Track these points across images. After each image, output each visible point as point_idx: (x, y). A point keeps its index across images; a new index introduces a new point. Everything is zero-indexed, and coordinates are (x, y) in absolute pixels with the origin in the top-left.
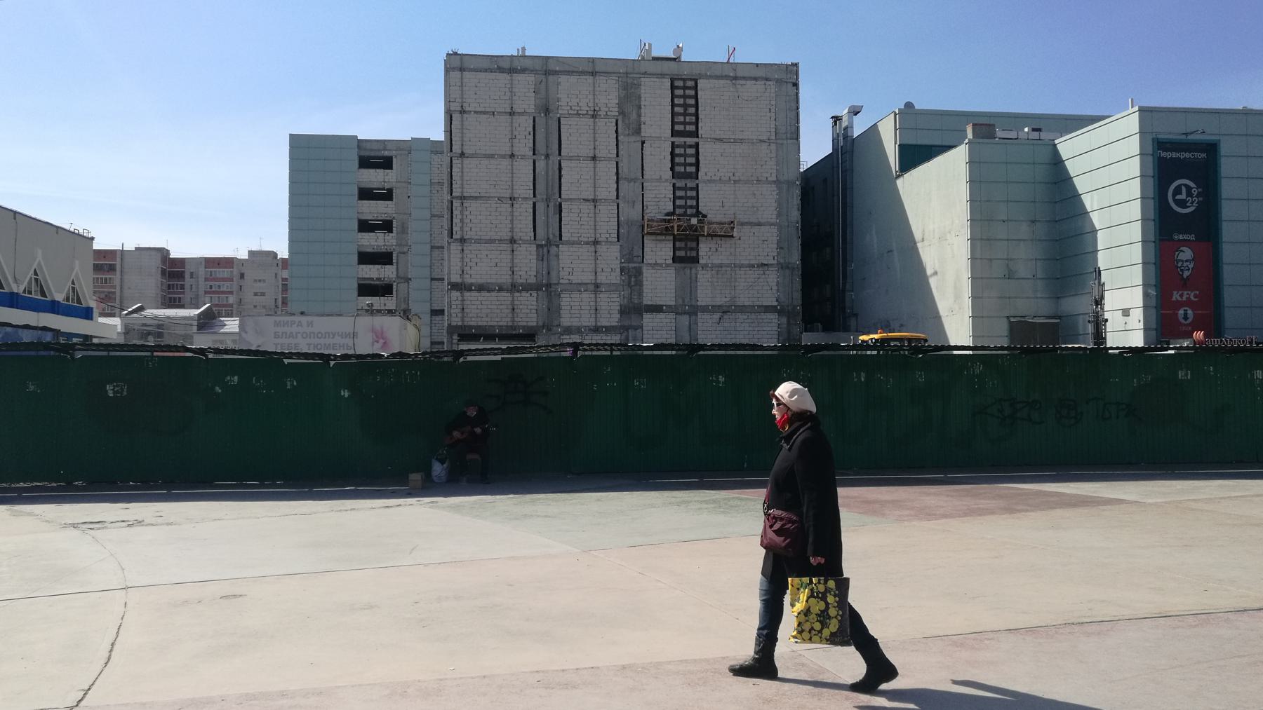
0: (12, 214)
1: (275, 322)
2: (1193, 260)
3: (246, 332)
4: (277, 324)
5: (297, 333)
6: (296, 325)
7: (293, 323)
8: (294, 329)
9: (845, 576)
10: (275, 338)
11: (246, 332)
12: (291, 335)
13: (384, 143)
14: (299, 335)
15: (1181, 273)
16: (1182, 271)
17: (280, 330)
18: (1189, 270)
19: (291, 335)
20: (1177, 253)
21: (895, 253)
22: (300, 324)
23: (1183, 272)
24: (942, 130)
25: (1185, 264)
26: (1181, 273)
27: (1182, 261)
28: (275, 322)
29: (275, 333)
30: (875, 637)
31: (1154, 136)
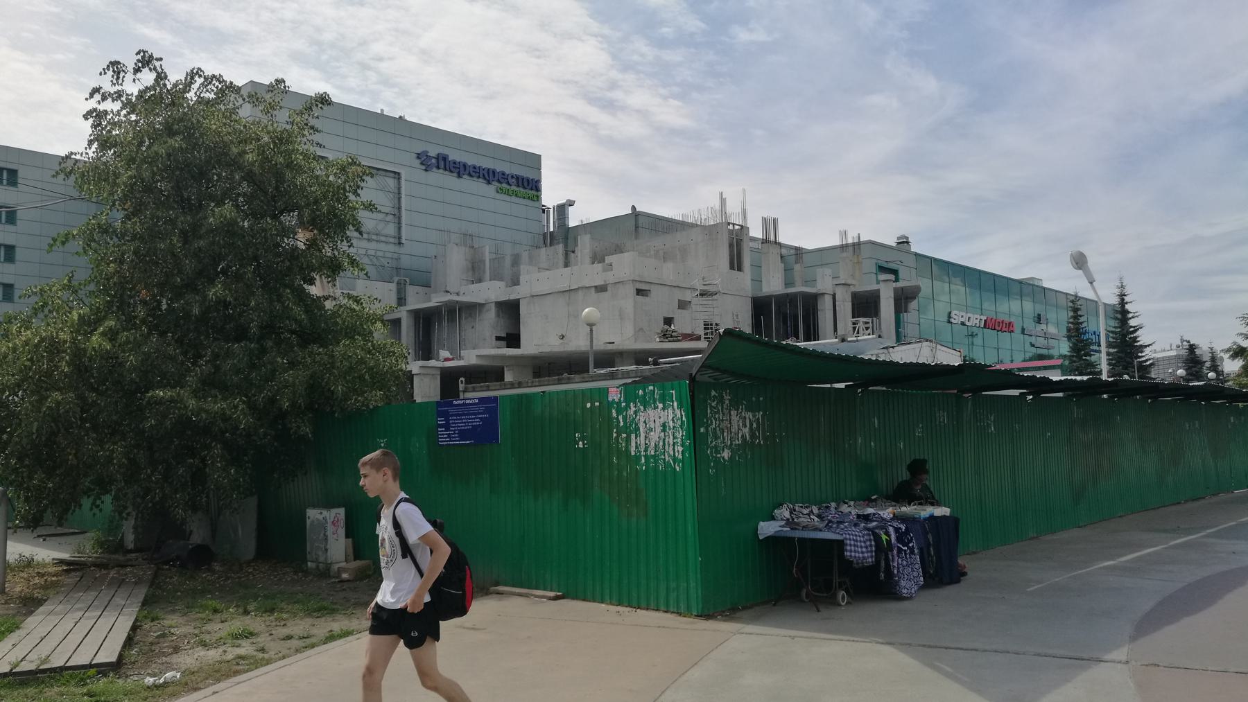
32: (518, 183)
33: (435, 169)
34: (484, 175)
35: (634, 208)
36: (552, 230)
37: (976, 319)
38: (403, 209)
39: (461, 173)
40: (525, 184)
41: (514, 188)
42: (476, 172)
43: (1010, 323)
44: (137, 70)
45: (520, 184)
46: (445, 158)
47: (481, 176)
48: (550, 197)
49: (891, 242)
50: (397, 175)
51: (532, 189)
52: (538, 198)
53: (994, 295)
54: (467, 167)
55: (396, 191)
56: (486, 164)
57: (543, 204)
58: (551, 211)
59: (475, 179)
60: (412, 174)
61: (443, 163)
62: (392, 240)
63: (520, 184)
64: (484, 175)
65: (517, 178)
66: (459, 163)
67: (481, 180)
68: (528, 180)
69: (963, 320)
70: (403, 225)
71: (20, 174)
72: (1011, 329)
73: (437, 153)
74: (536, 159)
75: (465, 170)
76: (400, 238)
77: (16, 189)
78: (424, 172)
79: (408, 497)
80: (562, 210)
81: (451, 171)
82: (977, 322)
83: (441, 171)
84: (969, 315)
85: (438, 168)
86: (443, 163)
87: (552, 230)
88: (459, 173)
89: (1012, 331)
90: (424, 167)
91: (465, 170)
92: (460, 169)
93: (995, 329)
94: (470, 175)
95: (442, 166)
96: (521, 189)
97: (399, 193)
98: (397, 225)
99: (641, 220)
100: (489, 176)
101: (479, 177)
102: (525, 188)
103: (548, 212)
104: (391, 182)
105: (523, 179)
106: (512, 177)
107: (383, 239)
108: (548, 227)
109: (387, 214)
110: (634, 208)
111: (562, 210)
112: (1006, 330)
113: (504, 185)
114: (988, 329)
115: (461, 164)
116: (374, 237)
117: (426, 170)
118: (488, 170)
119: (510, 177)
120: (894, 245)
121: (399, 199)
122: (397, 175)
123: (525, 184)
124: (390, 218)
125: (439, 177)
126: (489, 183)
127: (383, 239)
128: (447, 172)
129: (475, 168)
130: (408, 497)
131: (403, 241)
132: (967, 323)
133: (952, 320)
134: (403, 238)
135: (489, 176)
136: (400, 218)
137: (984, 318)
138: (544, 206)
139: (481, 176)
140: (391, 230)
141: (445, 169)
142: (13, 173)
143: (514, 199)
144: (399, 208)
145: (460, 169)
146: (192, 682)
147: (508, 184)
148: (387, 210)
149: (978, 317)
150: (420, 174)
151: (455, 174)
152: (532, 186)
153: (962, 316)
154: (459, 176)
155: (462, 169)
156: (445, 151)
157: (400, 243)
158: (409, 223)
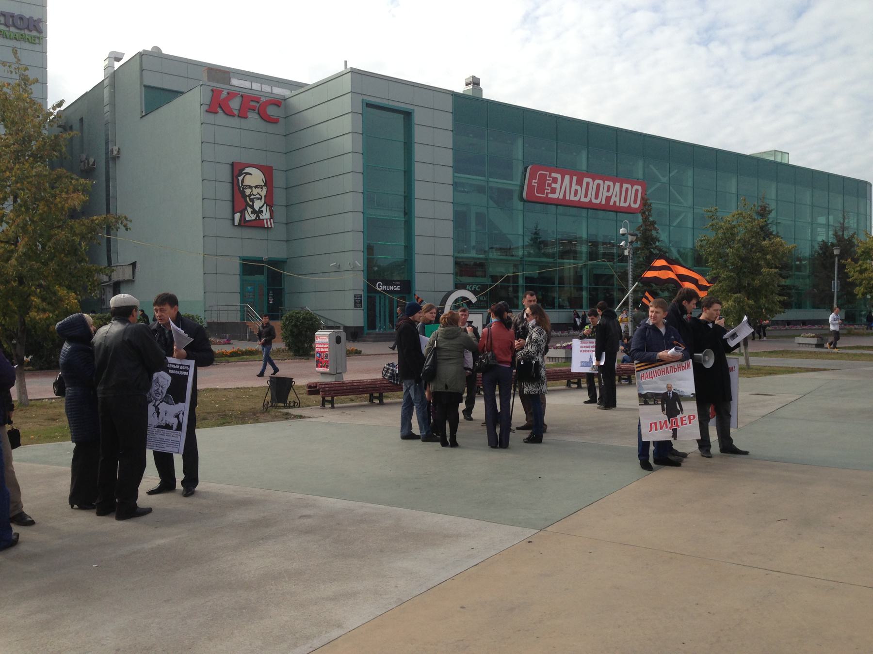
2: (265, 185)
15: (251, 203)
16: (252, 200)
18: (261, 199)
20: (240, 178)
23: (253, 203)
25: (255, 191)
26: (251, 203)
27: (251, 187)
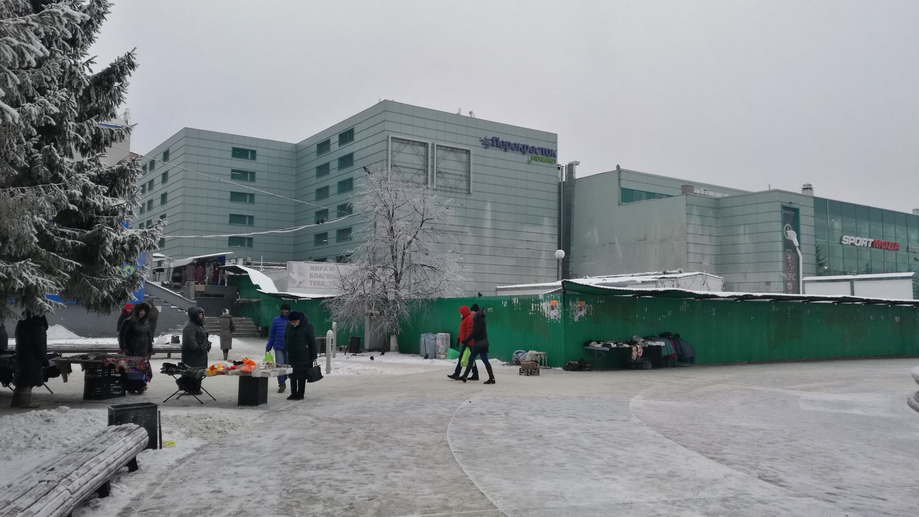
0: (898, 270)
1: (311, 267)
3: (293, 273)
4: (312, 268)
5: (323, 275)
6: (323, 269)
7: (321, 268)
8: (322, 272)
9: (84, 372)
10: (311, 277)
11: (293, 273)
12: (320, 276)
13: (654, 371)
14: (325, 276)
17: (314, 272)
19: (320, 276)
21: (618, 244)
22: (325, 269)
24: (185, 195)
28: (311, 267)
29: (311, 274)
30: (56, 378)
31: (183, 278)
32: (542, 153)
33: (491, 147)
34: (521, 149)
35: (618, 167)
36: (564, 180)
37: (864, 241)
38: (472, 172)
39: (507, 148)
40: (547, 153)
41: (539, 156)
42: (516, 148)
43: (895, 244)
44: (396, 285)
45: (544, 153)
46: (497, 140)
47: (519, 149)
48: (563, 160)
49: (798, 190)
50: (468, 152)
51: (551, 156)
52: (555, 161)
53: (881, 224)
54: (511, 145)
55: (468, 161)
56: (521, 141)
57: (558, 163)
58: (564, 168)
59: (515, 152)
60: (477, 151)
61: (496, 143)
62: (465, 192)
63: (544, 153)
64: (521, 149)
65: (542, 149)
66: (506, 142)
67: (518, 152)
68: (549, 151)
69: (852, 242)
70: (471, 164)
71: (258, 153)
72: (896, 248)
73: (492, 137)
74: (553, 138)
75: (509, 146)
76: (469, 190)
77: (254, 161)
78: (484, 149)
79: (471, 370)
80: (570, 167)
81: (500, 147)
82: (866, 243)
83: (494, 148)
84: (858, 238)
85: (493, 146)
86: (496, 143)
87: (564, 180)
88: (505, 148)
89: (898, 250)
90: (484, 146)
91: (509, 146)
92: (506, 146)
93: (881, 248)
94: (512, 149)
95: (495, 145)
96: (544, 157)
97: (469, 163)
98: (468, 182)
99: (623, 176)
100: (523, 149)
101: (518, 150)
102: (546, 155)
103: (562, 169)
104: (464, 156)
105: (545, 150)
106: (539, 149)
107: (459, 191)
108: (562, 179)
109: (462, 176)
110: (618, 167)
111: (570, 167)
112: (892, 248)
113: (534, 155)
114: (876, 247)
115: (507, 143)
116: (454, 190)
117: (486, 148)
118: (524, 145)
119: (537, 149)
120: (800, 191)
121: (470, 165)
122: (468, 152)
123: (547, 153)
124: (463, 178)
125: (493, 152)
126: (524, 153)
127: (459, 191)
128: (498, 149)
129: (515, 145)
130: (471, 370)
131: (471, 192)
132: (856, 244)
133: (843, 242)
134: (471, 190)
135: (523, 149)
136: (469, 177)
137: (872, 240)
138: (558, 165)
139: (519, 149)
140: (463, 185)
141: (497, 147)
142: (254, 152)
143: (540, 163)
144: (469, 172)
145: (506, 146)
146: (221, 438)
147: (536, 153)
148: (462, 173)
149: (867, 240)
150: (482, 151)
151: (503, 149)
152: (550, 154)
153: (852, 240)
154: (506, 150)
155: (507, 145)
156: (497, 136)
157: (469, 193)
158: (475, 172)
